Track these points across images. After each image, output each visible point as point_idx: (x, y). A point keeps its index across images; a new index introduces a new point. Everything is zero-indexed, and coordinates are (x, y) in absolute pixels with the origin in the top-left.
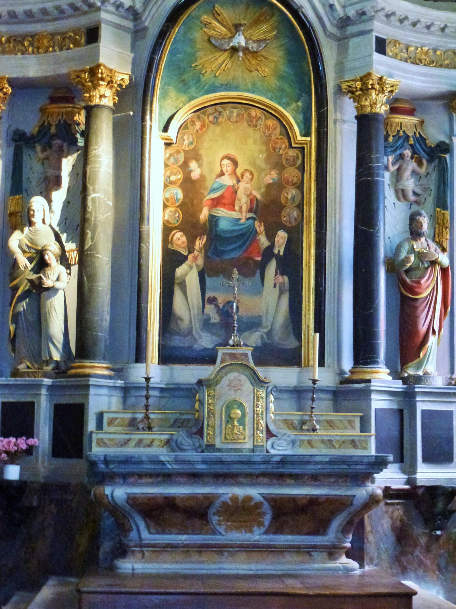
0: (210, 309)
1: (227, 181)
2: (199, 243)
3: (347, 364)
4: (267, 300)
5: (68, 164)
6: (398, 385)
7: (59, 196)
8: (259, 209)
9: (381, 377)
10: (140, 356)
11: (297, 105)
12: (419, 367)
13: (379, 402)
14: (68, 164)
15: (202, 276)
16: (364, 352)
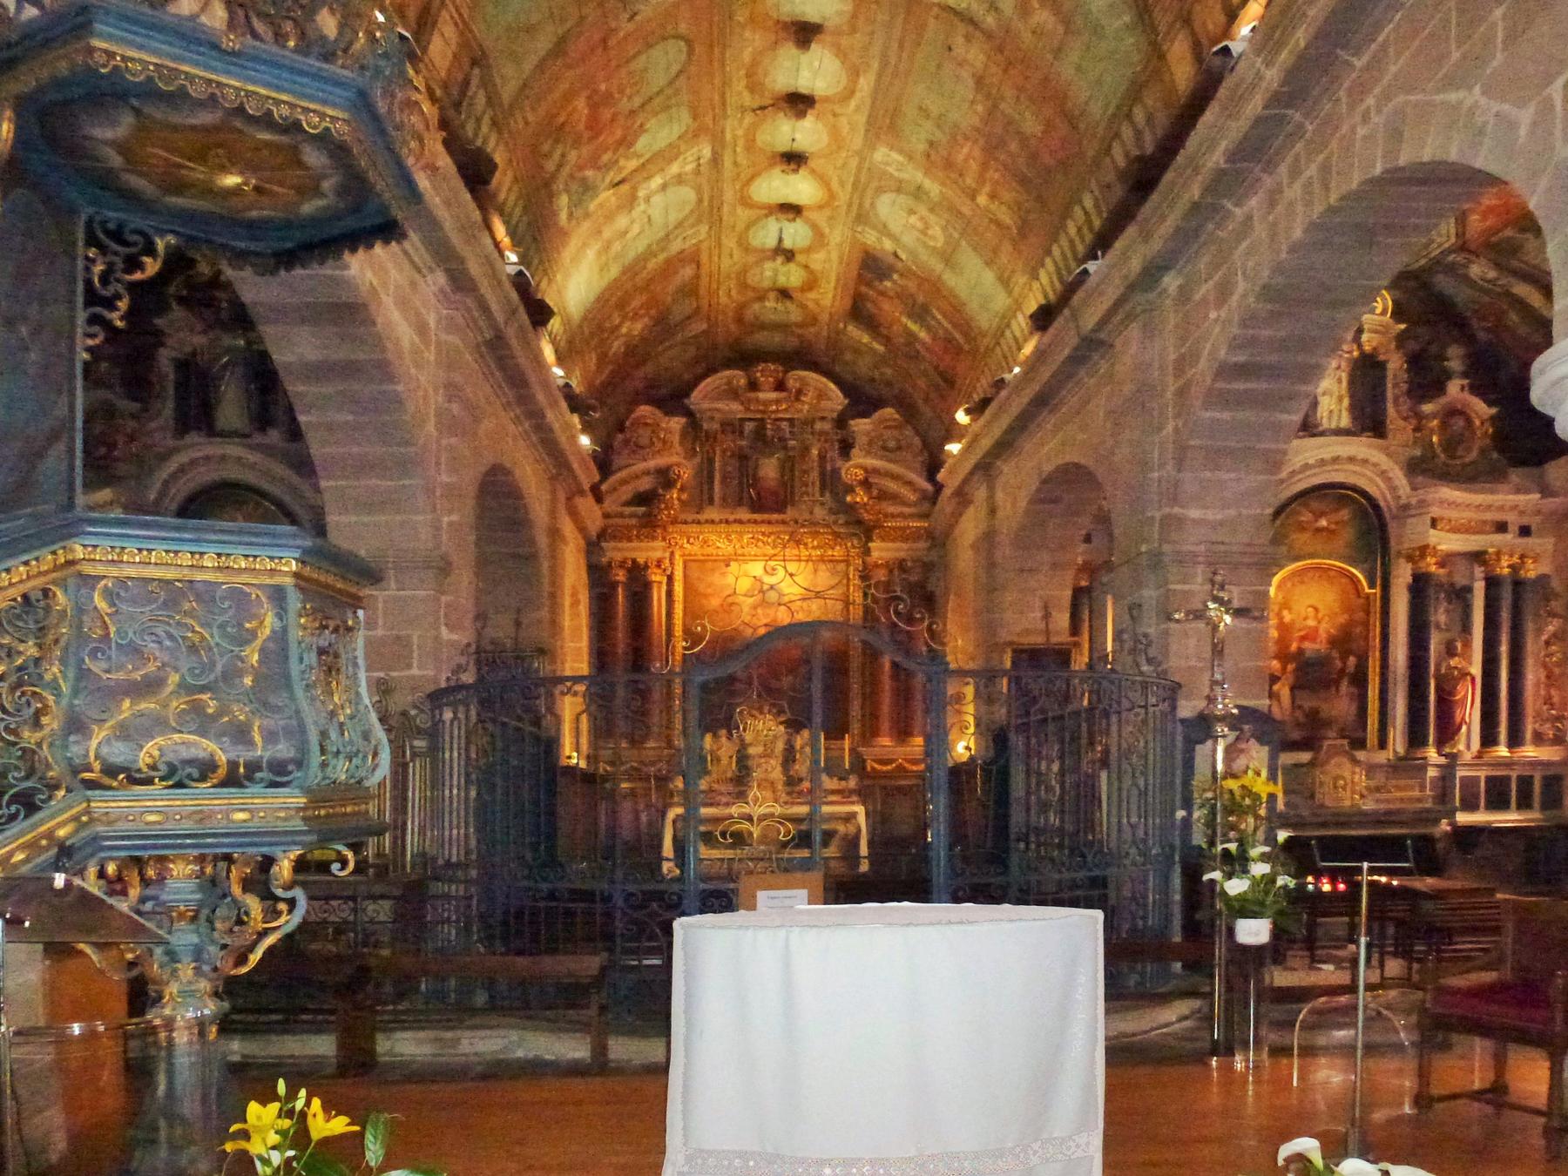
0: (1298, 714)
1: (1311, 623)
2: (1290, 667)
4: (1340, 706)
6: (1443, 760)
8: (1333, 642)
9: (1432, 753)
12: (1454, 746)
13: (1432, 773)
15: (1292, 689)
16: (1416, 738)
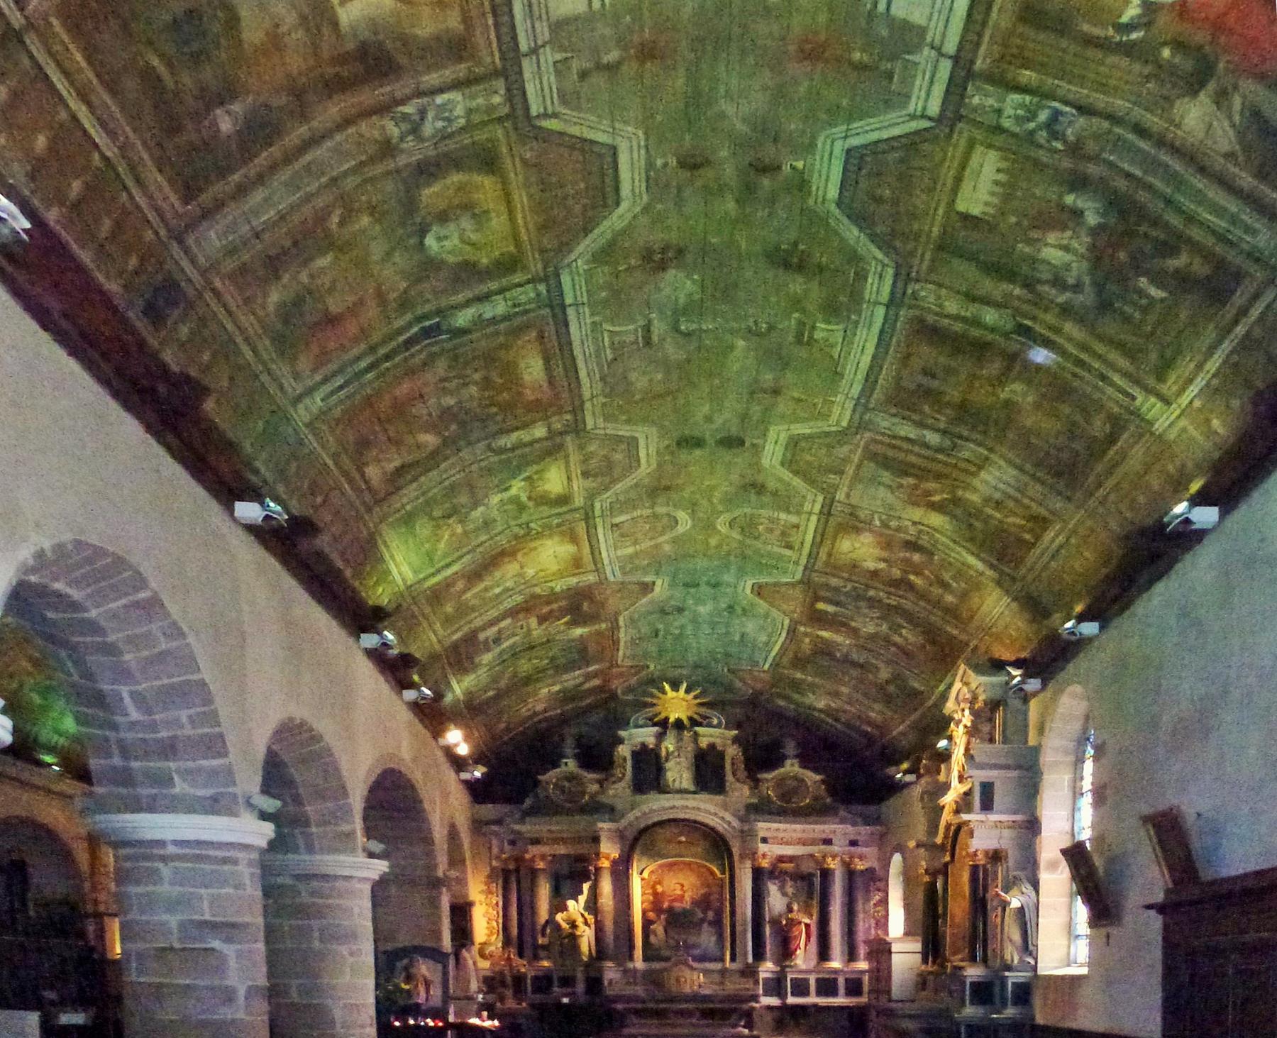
1: (679, 892)
3: (750, 960)
5: (586, 887)
7: (582, 899)
8: (695, 903)
10: (631, 958)
11: (415, 1020)
12: (222, 979)
14: (586, 887)
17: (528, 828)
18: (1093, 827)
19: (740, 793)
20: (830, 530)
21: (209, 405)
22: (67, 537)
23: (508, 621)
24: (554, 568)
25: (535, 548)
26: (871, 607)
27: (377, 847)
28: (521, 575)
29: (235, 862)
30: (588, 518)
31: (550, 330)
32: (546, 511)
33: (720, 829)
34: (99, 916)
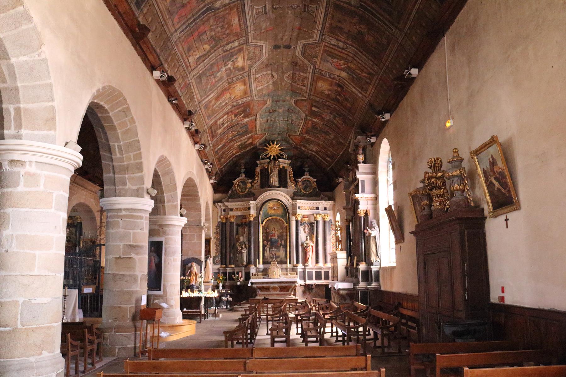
3: (295, 263)
17: (230, 205)
18: (394, 199)
19: (292, 188)
20: (315, 78)
21: (150, 36)
22: (107, 84)
23: (226, 116)
24: (239, 95)
25: (234, 88)
26: (328, 109)
27: (184, 212)
28: (230, 98)
29: (141, 218)
30: (249, 76)
31: (240, 9)
32: (238, 73)
33: (286, 203)
34: (100, 245)
